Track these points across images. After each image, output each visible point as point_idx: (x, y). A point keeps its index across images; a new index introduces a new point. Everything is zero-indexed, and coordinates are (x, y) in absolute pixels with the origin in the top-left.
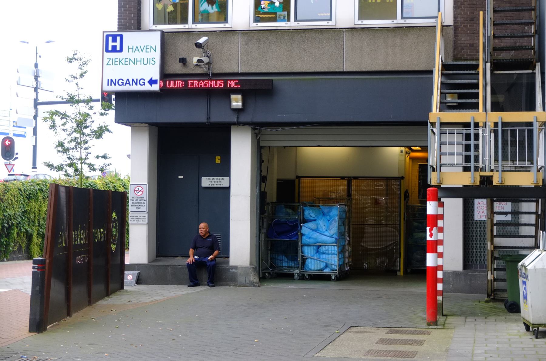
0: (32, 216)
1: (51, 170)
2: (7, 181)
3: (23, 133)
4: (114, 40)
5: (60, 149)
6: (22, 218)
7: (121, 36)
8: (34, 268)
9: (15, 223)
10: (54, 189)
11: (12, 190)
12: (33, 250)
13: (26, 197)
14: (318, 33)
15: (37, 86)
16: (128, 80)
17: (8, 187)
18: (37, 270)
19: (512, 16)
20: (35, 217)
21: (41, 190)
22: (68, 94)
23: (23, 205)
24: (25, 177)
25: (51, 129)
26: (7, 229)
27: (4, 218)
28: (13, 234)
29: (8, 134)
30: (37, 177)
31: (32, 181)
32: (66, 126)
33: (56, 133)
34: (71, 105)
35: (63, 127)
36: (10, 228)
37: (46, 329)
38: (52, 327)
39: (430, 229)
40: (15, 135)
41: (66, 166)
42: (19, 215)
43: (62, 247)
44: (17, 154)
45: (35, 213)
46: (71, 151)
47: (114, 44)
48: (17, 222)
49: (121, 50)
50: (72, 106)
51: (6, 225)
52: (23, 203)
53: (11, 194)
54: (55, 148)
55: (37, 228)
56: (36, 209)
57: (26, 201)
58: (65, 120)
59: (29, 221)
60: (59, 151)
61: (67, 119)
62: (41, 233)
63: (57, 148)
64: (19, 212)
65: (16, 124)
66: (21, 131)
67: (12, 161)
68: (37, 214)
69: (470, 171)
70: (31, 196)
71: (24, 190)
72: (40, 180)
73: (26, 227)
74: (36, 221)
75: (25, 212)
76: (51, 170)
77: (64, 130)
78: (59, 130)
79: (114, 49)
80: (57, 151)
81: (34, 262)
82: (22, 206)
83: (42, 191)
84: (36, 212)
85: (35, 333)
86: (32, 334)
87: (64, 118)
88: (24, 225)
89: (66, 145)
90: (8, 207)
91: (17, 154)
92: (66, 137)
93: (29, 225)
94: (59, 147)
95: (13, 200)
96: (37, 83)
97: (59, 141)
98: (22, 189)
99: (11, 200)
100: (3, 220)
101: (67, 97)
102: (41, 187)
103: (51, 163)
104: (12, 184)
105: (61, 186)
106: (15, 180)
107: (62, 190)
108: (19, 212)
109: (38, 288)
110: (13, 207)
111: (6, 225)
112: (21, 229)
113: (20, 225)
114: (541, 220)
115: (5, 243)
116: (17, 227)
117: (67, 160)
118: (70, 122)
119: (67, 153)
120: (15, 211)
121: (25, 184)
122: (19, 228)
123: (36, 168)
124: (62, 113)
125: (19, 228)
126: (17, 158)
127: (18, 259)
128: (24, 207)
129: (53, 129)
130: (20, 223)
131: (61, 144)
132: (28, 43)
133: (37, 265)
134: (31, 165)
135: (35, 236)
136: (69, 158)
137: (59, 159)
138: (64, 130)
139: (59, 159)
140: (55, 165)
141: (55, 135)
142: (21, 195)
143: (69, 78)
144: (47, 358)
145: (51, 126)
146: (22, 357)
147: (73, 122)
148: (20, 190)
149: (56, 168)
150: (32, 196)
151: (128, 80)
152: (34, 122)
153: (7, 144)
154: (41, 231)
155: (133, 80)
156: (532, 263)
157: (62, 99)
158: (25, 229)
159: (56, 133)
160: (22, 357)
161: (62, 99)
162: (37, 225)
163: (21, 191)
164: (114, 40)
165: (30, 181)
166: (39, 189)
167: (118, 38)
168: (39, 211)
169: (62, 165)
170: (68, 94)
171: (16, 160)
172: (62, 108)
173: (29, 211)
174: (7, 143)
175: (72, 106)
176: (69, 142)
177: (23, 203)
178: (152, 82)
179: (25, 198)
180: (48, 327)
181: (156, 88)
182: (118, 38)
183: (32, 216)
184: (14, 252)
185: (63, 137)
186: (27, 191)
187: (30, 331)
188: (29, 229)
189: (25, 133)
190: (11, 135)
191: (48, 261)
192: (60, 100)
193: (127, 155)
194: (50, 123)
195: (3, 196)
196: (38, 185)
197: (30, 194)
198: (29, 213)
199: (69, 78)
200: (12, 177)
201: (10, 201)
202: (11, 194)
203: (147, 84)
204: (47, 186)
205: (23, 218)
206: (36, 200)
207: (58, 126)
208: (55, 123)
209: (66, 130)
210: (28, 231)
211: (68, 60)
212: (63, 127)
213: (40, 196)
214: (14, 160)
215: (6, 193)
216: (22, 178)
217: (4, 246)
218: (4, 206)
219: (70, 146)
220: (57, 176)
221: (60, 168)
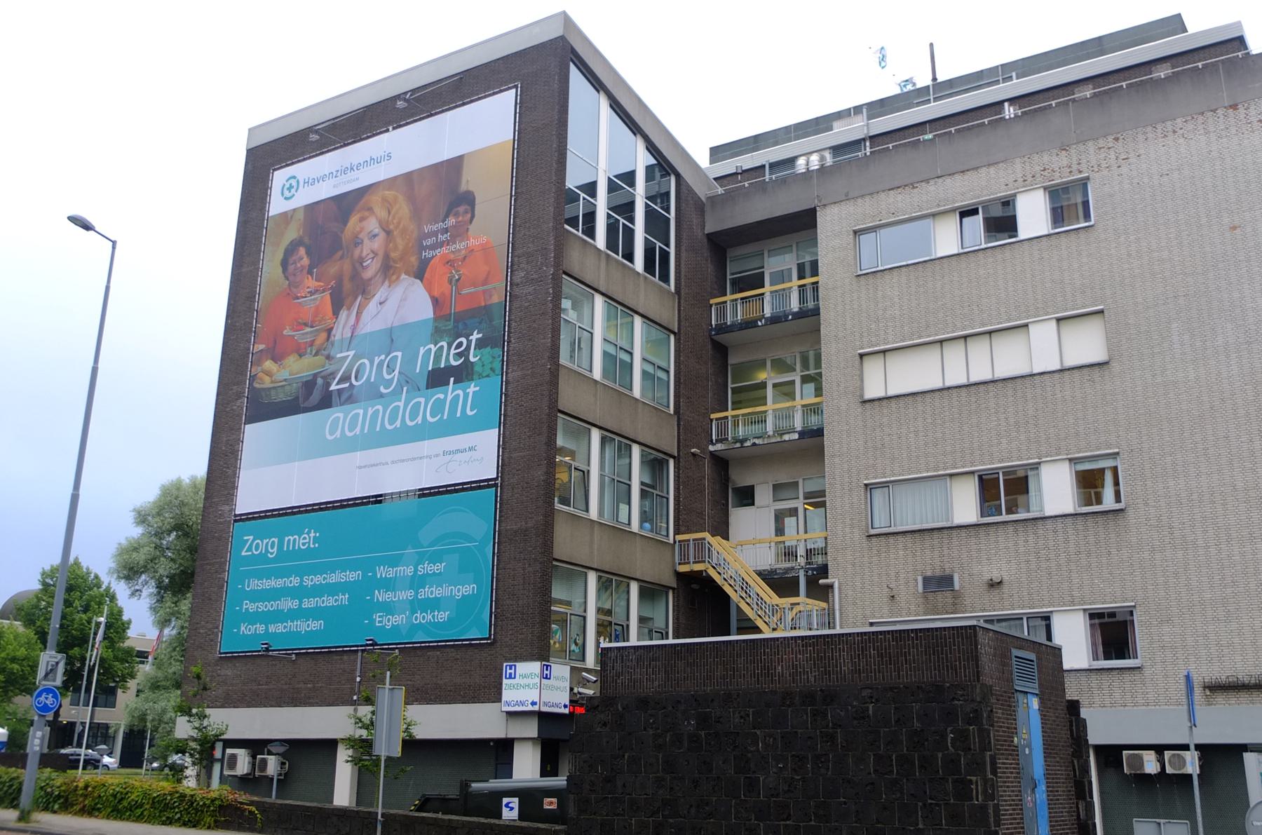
4: (510, 674)
7: (515, 666)
14: (138, 563)
16: (517, 701)
19: (108, 776)
47: (511, 671)
49: (515, 678)
69: (777, 535)
79: (510, 677)
114: (376, 428)
151: (517, 701)
155: (521, 702)
156: (117, 250)
164: (510, 674)
167: (513, 667)
178: (565, 706)
181: (567, 711)
182: (513, 667)
203: (530, 706)
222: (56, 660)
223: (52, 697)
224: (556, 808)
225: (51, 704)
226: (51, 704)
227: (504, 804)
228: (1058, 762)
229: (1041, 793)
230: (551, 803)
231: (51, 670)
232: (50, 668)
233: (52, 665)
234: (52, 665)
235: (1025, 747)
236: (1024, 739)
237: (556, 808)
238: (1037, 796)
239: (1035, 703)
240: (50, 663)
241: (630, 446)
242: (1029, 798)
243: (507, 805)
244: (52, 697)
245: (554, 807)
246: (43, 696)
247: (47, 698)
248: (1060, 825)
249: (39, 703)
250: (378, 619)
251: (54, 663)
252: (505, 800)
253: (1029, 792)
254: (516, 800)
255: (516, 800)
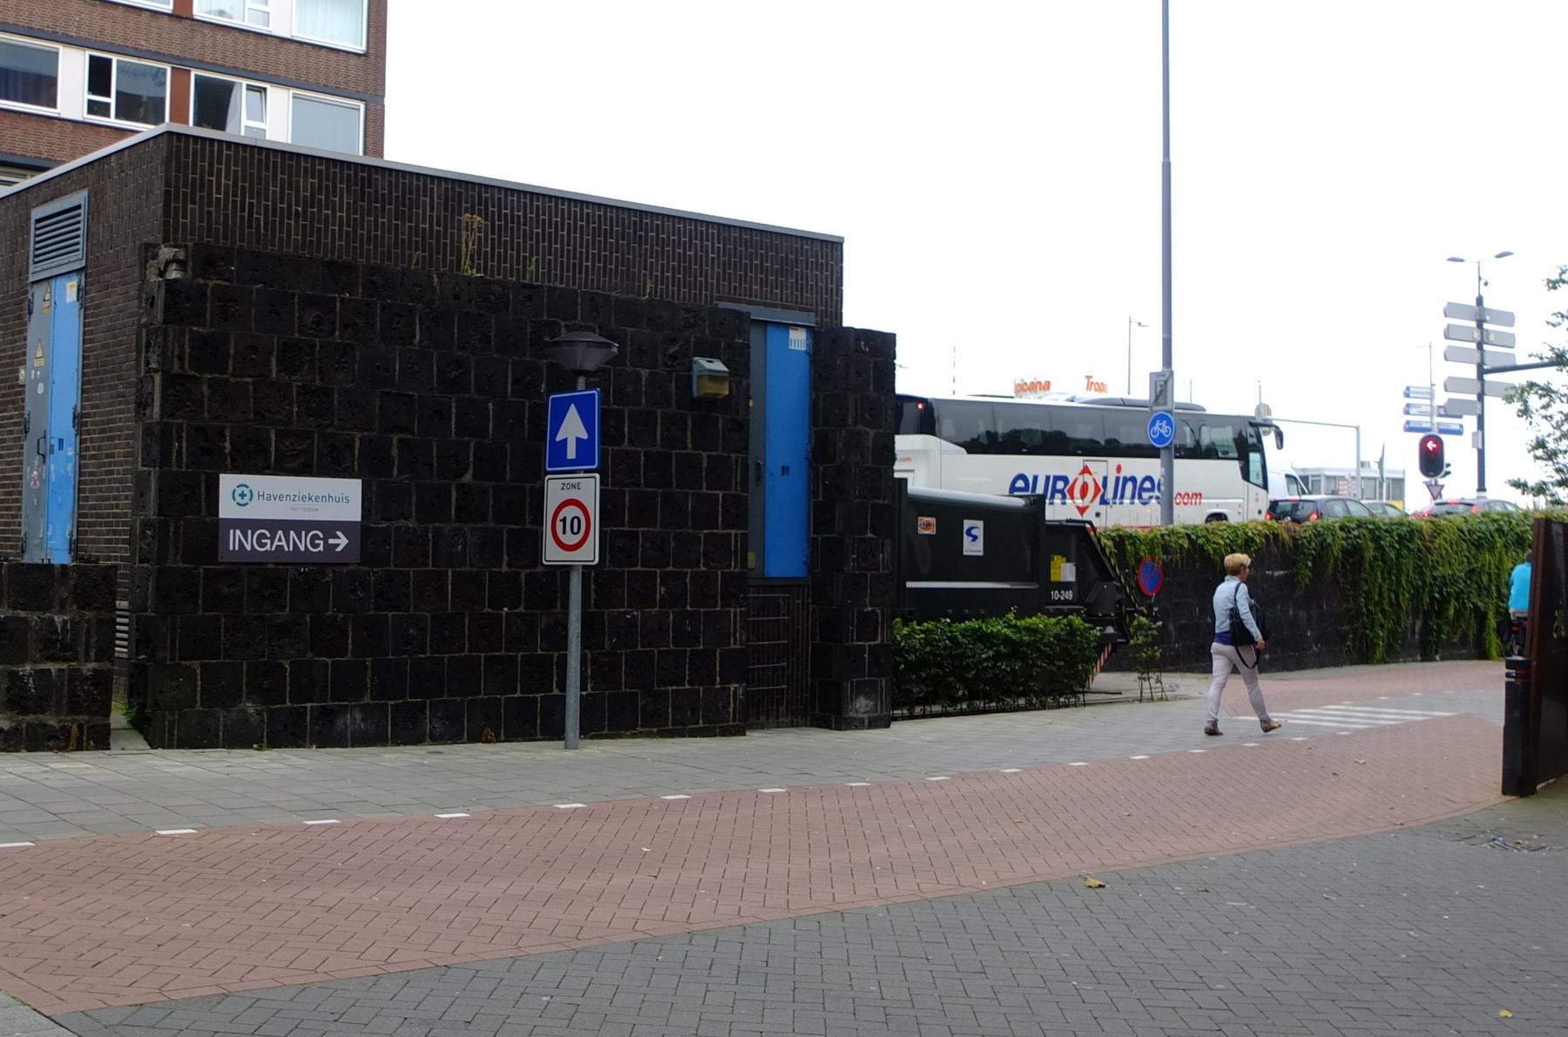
0: (1485, 579)
1: (1523, 493)
2: (1436, 516)
3: (1458, 428)
5: (1540, 452)
6: (1465, 582)
8: (1508, 675)
9: (1452, 591)
10: (1542, 530)
11: (1446, 531)
12: (1488, 642)
13: (1473, 544)
15: (1482, 338)
17: (1439, 526)
18: (1513, 680)
20: (1490, 580)
21: (1500, 530)
22: (1552, 349)
23: (1468, 558)
24: (1467, 507)
25: (1522, 416)
26: (1440, 603)
27: (1432, 582)
28: (1448, 609)
29: (1430, 430)
30: (1490, 508)
31: (1483, 515)
32: (1549, 409)
33: (1531, 423)
34: (1558, 370)
35: (1543, 412)
36: (1444, 601)
37: (1536, 791)
38: (1545, 787)
39: (1098, 443)
40: (1442, 431)
41: (1552, 484)
42: (1461, 578)
43: (1560, 637)
44: (1448, 465)
45: (1489, 574)
46: (1560, 456)
48: (1457, 589)
50: (1561, 370)
51: (1437, 595)
52: (1467, 554)
53: (1445, 539)
54: (1529, 451)
55: (1495, 600)
56: (1493, 566)
57: (1474, 551)
58: (1546, 399)
59: (1480, 588)
60: (1537, 458)
61: (1551, 397)
62: (1503, 611)
63: (1532, 453)
64: (1460, 571)
65: (1445, 411)
66: (1453, 423)
67: (1441, 481)
68: (1493, 576)
70: (1481, 541)
71: (1469, 531)
72: (1498, 514)
73: (1475, 600)
74: (1493, 588)
75: (1472, 571)
76: (1523, 493)
77: (1545, 417)
78: (1536, 418)
80: (1533, 459)
81: (1509, 665)
82: (1465, 560)
83: (1503, 532)
84: (1492, 572)
85: (1513, 797)
86: (1508, 798)
87: (1545, 396)
88: (1471, 595)
89: (1551, 445)
90: (1441, 563)
91: (1448, 465)
92: (1551, 430)
93: (1479, 596)
94: (1537, 449)
95: (1449, 549)
96: (1482, 333)
97: (1537, 438)
98: (1465, 529)
99: (1445, 549)
100: (1432, 587)
101: (1550, 354)
102: (1500, 526)
103: (1522, 481)
104: (1445, 519)
105: (1555, 522)
106: (1449, 513)
107: (1557, 529)
108: (1460, 571)
109: (1517, 713)
110: (1450, 563)
111: (1437, 595)
112: (1464, 603)
113: (1462, 595)
115: (1435, 627)
116: (1457, 600)
117: (1554, 474)
118: (1557, 401)
119: (1555, 461)
120: (1456, 569)
121: (1471, 519)
122: (1461, 601)
123: (1484, 490)
124: (1542, 384)
125: (1461, 601)
126: (1448, 473)
127: (1462, 658)
128: (1469, 563)
129: (1525, 417)
130: (1462, 591)
131: (1541, 444)
132: (1479, 263)
133: (1513, 671)
134: (1475, 485)
135: (1491, 615)
136: (1559, 471)
137: (1541, 472)
138: (1545, 417)
139: (1541, 472)
140: (1531, 483)
141: (1530, 427)
142: (1464, 540)
143: (1555, 320)
144: (1543, 845)
145: (1520, 411)
146: (1494, 840)
147: (1562, 402)
148: (1462, 532)
149: (1533, 489)
150: (1484, 542)
152: (1479, 406)
153: (1431, 449)
154: (1503, 608)
157: (1541, 358)
158: (1473, 603)
159: (1531, 423)
160: (1494, 840)
161: (1541, 358)
162: (1495, 595)
163: (1464, 534)
165: (1479, 515)
166: (1497, 530)
168: (1498, 569)
169: (1544, 483)
170: (1552, 349)
171: (1448, 477)
172: (1542, 376)
173: (1478, 570)
174: (1431, 445)
175: (1561, 370)
176: (1555, 439)
177: (1467, 554)
179: (1470, 546)
180: (1538, 787)
183: (1485, 579)
184: (1454, 646)
185: (1545, 429)
186: (1474, 533)
187: (1505, 792)
188: (1479, 604)
189: (1461, 426)
190: (1435, 432)
191: (1534, 663)
192: (1537, 361)
193: (1087, 389)
194: (1517, 405)
195: (1430, 541)
196: (1494, 521)
197: (1480, 538)
198: (1480, 573)
199: (1555, 320)
200: (1445, 508)
201: (1444, 552)
202: (1445, 539)
204: (1510, 523)
205: (1469, 582)
206: (1492, 549)
207: (1534, 411)
208: (1529, 404)
209: (1551, 417)
210: (1477, 606)
211: (1548, 283)
212: (1543, 412)
213: (1500, 542)
214: (1444, 476)
215: (1435, 537)
216: (1461, 507)
217: (1435, 634)
218: (1432, 561)
219: (1559, 447)
220: (1525, 502)
221: (1540, 489)
222: (1164, 379)
223: (1167, 425)
224: (934, 533)
225: (1167, 434)
226: (1167, 434)
227: (965, 529)
228: (120, 395)
229: (64, 464)
230: (928, 525)
231: (1161, 392)
232: (1159, 389)
233: (1161, 386)
234: (1161, 386)
235: (37, 381)
236: (36, 369)
237: (934, 533)
238: (52, 468)
239: (69, 290)
240: (1159, 383)
241: (265, 89)
242: (35, 473)
243: (969, 533)
244: (1167, 425)
245: (932, 531)
246: (1157, 424)
247: (1161, 427)
248: (108, 524)
249: (1154, 434)
250: (747, 298)
251: (1162, 383)
252: (967, 524)
253: (36, 462)
254: (980, 524)
255: (980, 524)
